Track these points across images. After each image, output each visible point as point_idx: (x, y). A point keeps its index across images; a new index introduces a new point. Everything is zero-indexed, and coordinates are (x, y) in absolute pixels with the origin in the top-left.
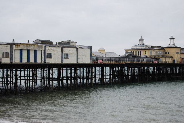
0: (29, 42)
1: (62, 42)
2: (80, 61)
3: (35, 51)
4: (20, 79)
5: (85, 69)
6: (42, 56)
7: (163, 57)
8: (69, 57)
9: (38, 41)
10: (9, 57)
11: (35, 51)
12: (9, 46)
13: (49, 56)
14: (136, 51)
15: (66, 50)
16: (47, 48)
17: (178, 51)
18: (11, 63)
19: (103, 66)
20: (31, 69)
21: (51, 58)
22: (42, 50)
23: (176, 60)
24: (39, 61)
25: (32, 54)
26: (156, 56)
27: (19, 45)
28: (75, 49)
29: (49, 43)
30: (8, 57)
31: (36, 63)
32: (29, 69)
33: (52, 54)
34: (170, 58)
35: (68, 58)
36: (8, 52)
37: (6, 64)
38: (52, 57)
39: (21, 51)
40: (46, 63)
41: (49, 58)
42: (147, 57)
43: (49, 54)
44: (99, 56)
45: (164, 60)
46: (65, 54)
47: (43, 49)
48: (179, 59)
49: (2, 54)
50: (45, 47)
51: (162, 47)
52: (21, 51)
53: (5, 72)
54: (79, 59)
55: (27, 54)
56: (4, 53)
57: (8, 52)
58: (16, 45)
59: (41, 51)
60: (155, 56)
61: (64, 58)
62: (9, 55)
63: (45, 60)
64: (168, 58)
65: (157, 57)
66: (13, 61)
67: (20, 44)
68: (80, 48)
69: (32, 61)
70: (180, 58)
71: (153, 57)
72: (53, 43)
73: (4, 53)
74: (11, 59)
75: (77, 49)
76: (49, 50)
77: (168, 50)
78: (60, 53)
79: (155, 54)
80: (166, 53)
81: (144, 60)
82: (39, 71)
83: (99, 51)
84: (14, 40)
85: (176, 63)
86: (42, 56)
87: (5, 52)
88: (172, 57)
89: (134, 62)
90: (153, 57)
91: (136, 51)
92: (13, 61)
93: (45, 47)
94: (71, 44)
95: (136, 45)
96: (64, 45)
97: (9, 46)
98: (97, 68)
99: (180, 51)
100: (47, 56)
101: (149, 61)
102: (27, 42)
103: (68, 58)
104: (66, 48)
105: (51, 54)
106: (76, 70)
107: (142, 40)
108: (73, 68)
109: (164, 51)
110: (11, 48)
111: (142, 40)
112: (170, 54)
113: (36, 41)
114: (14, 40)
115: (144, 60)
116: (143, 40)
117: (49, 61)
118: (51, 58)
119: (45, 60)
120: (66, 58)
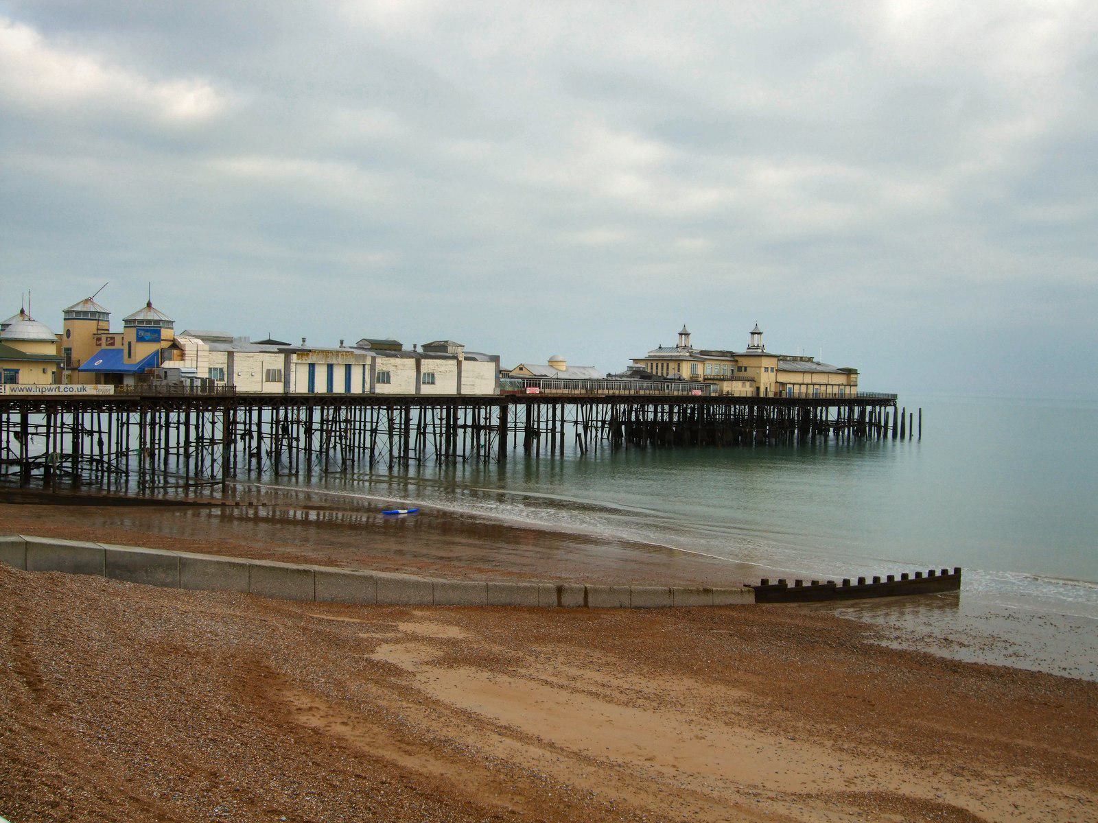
0: (344, 345)
1: (432, 343)
2: (466, 391)
3: (348, 368)
4: (62, 433)
5: (600, 406)
6: (364, 378)
7: (732, 379)
8: (436, 381)
9: (366, 343)
10: (283, 380)
11: (348, 368)
12: (282, 356)
13: (385, 378)
14: (662, 364)
15: (428, 365)
16: (379, 360)
17: (770, 366)
18: (286, 393)
19: (530, 401)
20: (295, 408)
21: (388, 382)
22: (364, 366)
23: (762, 389)
24: (356, 389)
25: (339, 374)
26: (709, 377)
27: (308, 355)
28: (454, 362)
29: (390, 348)
30: (280, 381)
31: (348, 395)
32: (353, 407)
33: (392, 374)
34: (748, 384)
35: (433, 383)
36: (279, 368)
37: (273, 395)
38: (392, 379)
39: (312, 367)
40: (374, 393)
41: (383, 382)
42: (680, 379)
43: (383, 373)
44: (545, 376)
45: (727, 387)
46: (424, 374)
47: (369, 362)
48: (773, 385)
49: (264, 375)
50: (374, 359)
51: (732, 355)
52: (312, 367)
53: (282, 413)
54: (462, 386)
55: (326, 373)
56: (268, 371)
57: (280, 370)
58: (298, 355)
59: (362, 367)
60: (706, 377)
61: (424, 383)
62: (283, 377)
63: (372, 387)
64: (740, 383)
65: (710, 379)
66: (292, 390)
67: (310, 351)
68: (466, 359)
69: (339, 388)
70: (777, 382)
71: (701, 379)
72: (404, 348)
73: (268, 371)
74: (287, 384)
75: (459, 364)
76: (383, 363)
77: (744, 362)
78: (414, 373)
79: (708, 372)
80: (740, 369)
81: (668, 386)
82: (397, 409)
83: (550, 364)
84: (304, 340)
85: (762, 395)
86: (364, 378)
87: (273, 370)
88: (752, 380)
89: (642, 392)
90: (701, 379)
91: (662, 364)
92: (316, 391)
93: (374, 359)
94: (450, 349)
95: (660, 348)
96: (437, 350)
97: (282, 356)
98: (543, 407)
99: (774, 366)
100: (378, 378)
101: (608, 389)
102: (336, 346)
103: (433, 383)
104: (429, 360)
105: (388, 373)
106: (337, 410)
107: (684, 334)
108: (314, 407)
109: (734, 363)
110: (287, 363)
111: (684, 334)
112: (750, 373)
113: (361, 343)
114: (304, 340)
115: (668, 386)
116: (687, 334)
117: (381, 389)
118: (388, 382)
119: (372, 387)
120: (428, 383)
